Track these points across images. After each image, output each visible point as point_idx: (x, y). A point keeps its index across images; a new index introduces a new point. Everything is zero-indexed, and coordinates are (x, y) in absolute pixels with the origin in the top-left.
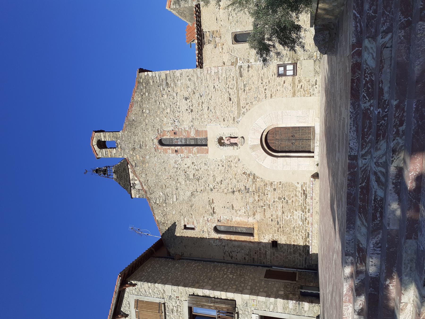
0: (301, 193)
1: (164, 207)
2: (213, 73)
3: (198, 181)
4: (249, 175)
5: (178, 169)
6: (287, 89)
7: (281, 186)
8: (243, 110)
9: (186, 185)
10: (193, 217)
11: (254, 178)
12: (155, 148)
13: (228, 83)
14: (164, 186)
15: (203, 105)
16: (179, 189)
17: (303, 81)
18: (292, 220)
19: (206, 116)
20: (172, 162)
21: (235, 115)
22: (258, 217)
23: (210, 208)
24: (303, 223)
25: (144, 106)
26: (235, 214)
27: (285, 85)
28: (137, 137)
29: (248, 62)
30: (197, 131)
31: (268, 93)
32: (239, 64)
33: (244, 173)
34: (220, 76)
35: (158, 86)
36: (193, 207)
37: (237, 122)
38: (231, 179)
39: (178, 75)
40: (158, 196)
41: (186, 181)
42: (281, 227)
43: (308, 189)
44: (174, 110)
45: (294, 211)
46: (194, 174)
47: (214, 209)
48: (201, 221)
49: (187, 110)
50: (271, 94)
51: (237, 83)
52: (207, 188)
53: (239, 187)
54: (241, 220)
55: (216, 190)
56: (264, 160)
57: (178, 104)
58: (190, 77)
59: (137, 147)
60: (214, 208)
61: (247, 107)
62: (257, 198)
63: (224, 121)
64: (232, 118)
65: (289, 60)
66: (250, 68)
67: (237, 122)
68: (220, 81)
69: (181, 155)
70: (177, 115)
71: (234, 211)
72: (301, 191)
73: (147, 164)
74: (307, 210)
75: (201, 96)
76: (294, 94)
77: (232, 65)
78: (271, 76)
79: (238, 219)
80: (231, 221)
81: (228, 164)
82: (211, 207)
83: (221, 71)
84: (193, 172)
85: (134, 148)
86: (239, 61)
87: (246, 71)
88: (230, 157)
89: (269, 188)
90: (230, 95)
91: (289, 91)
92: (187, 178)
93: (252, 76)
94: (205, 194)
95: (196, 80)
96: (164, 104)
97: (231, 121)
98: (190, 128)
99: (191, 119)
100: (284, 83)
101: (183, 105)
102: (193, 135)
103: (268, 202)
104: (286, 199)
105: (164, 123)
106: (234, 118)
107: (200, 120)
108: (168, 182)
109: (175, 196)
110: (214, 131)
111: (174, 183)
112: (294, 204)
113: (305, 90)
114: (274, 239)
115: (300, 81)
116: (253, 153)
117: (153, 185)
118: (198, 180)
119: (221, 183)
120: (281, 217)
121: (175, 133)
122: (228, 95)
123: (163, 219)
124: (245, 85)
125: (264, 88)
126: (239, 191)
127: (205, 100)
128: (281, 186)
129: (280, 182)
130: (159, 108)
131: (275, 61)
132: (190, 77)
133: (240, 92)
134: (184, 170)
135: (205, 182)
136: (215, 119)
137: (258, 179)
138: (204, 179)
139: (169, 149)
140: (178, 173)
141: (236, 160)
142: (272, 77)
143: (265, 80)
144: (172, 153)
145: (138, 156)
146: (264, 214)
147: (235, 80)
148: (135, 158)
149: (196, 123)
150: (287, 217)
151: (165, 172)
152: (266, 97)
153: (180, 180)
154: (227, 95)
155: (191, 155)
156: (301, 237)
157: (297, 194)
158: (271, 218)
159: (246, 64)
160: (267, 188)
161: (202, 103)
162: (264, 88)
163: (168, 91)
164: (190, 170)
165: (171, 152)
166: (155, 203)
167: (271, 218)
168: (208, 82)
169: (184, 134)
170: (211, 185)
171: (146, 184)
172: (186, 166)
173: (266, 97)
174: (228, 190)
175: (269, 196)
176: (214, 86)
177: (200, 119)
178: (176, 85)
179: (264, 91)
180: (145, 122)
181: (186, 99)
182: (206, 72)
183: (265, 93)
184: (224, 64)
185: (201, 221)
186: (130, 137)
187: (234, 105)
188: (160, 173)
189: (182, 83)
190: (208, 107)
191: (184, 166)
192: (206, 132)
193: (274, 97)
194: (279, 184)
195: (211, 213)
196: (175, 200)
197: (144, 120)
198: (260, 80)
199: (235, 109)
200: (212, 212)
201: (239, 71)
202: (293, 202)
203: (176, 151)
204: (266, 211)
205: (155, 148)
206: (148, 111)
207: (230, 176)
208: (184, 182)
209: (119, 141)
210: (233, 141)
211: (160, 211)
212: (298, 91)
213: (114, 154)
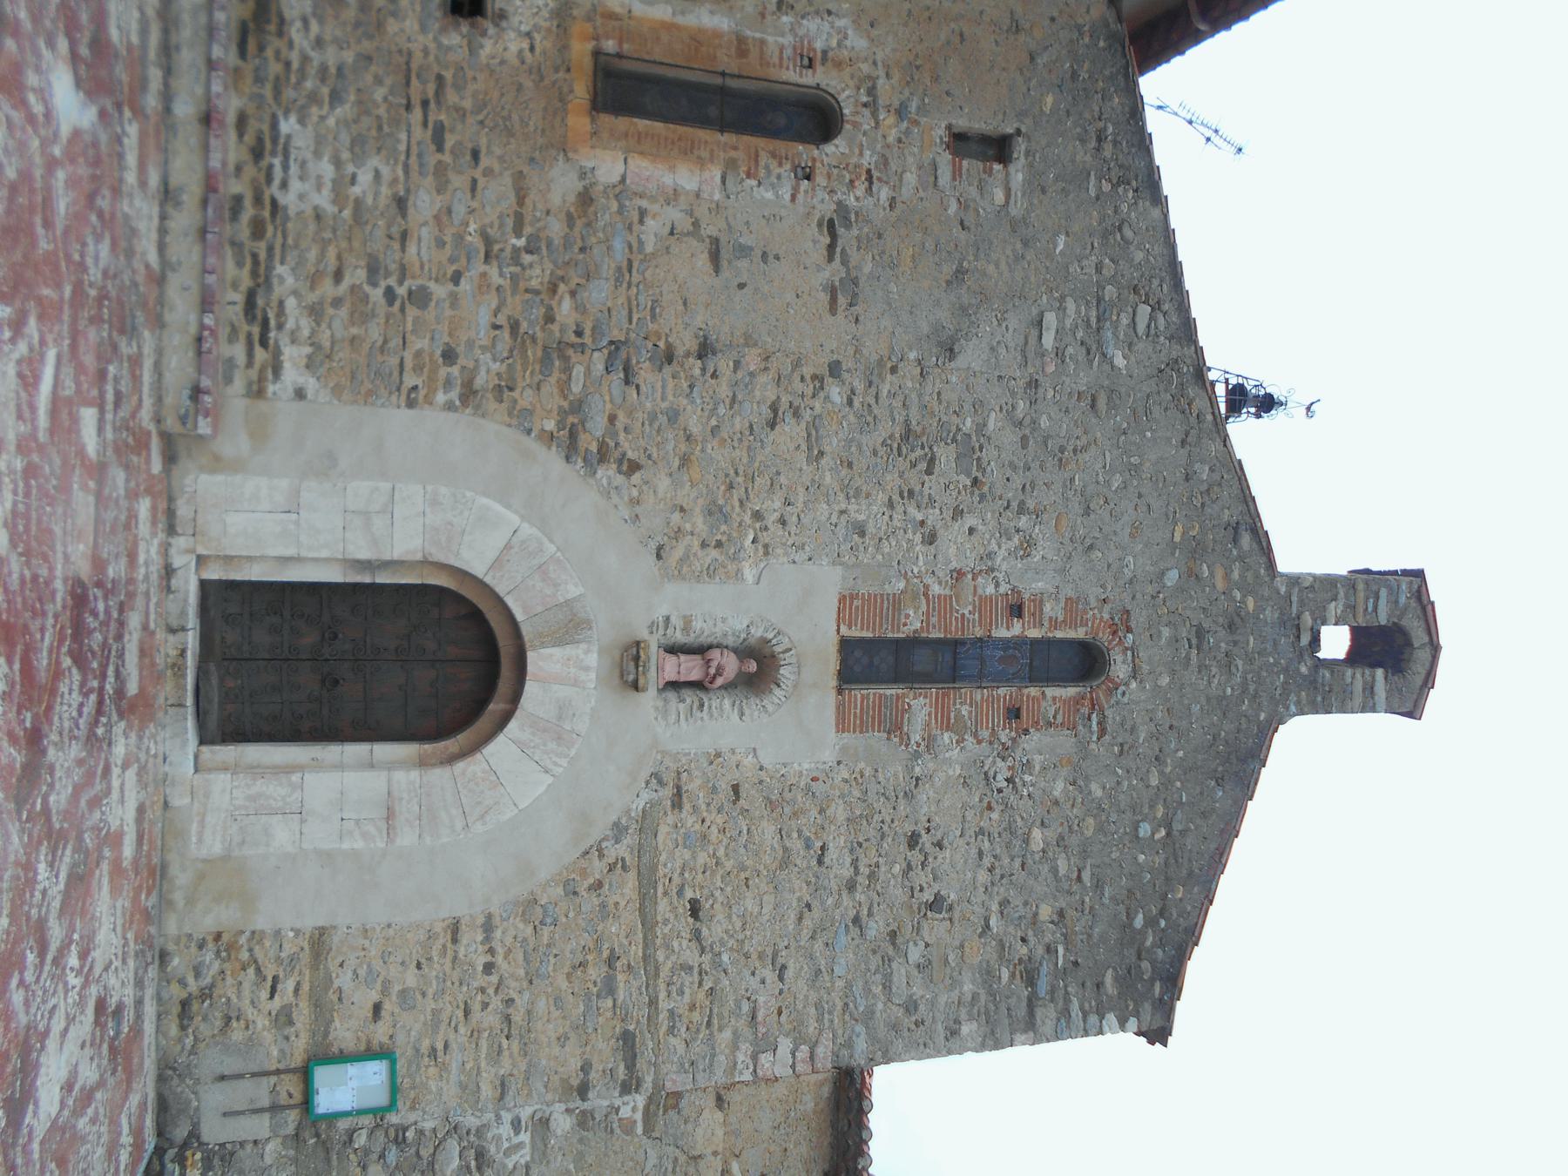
0: (280, 327)
1: (1113, 280)
2: (785, 1045)
3: (907, 422)
4: (603, 455)
5: (1014, 504)
6: (362, 972)
7: (410, 380)
8: (621, 850)
9: (978, 406)
10: (953, 207)
11: (573, 435)
12: (1129, 630)
13: (701, 995)
14: (1102, 403)
15: (847, 872)
16: (1021, 383)
17: (262, 1022)
18: (346, 155)
19: (839, 811)
20: (1045, 549)
21: (670, 819)
22: (561, 184)
23: (854, 256)
24: (274, 126)
25: (1158, 861)
26: (701, 211)
27: (374, 996)
28: (1214, 689)
29: (583, 1112)
30: (895, 728)
31: (471, 947)
32: (640, 1100)
33: (634, 467)
34: (747, 1032)
35: (1076, 964)
36: (948, 269)
37: (661, 782)
38: (715, 431)
39: (974, 1025)
40: (1140, 346)
41: (981, 427)
42: (417, 114)
43: (238, 352)
44: (1008, 846)
45: (330, 209)
46: (929, 472)
47: (831, 248)
48: (911, 178)
49: (939, 845)
50: (455, 941)
51: (653, 1002)
52: (859, 386)
53: (671, 383)
54: (672, 169)
55: (807, 371)
56: (508, 546)
57: (983, 876)
58: (908, 1022)
59: (1218, 640)
60: (830, 259)
61: (598, 867)
62: (565, 309)
63: (736, 789)
64: (687, 807)
65: (351, 1134)
66: (575, 1082)
67: (661, 782)
68: (746, 1007)
69: (990, 590)
70: (995, 816)
71: (711, 231)
72: (284, 341)
73: (1177, 538)
74: (248, 212)
75: (856, 920)
76: (319, 941)
77: (678, 1095)
78: (454, 1046)
79: (686, 178)
80: (731, 165)
81: (720, 533)
82: (844, 262)
83: (741, 1057)
84: (933, 485)
85: (1231, 627)
86: (639, 1116)
87: (597, 1067)
88: (711, 572)
89: (488, 371)
90: (697, 936)
91: (352, 962)
92: (969, 451)
93: (562, 1040)
94: (873, 349)
95: (880, 1006)
96: (1054, 871)
97: (693, 785)
98: (930, 742)
99: (925, 794)
100: (377, 1009)
101: (956, 870)
102: (920, 706)
103: (496, 279)
104: (377, 294)
105: (1064, 772)
106: (677, 803)
107: (873, 788)
108: (1079, 432)
109: (1049, 340)
110: (797, 732)
111: (1044, 422)
112: (332, 253)
113: (251, 971)
114: (465, 28)
115: (284, 1018)
116: (573, 590)
117: (1157, 412)
118: (908, 434)
119: (774, 408)
120: (414, 175)
121: (1014, 713)
122: (705, 932)
123: (1124, 208)
124: (609, 988)
125: (494, 979)
126: (669, 357)
127: (837, 905)
128: (410, 380)
129: (411, 404)
130: (1084, 854)
131: (428, 1125)
132: (908, 1022)
133: (636, 951)
134: (982, 497)
135: (867, 421)
136: (787, 796)
137: (550, 425)
138: (882, 432)
139: (1054, 624)
140: (1017, 481)
141: (679, 552)
142: (452, 1036)
143: (491, 1019)
144: (1039, 601)
145: (1220, 585)
146: (521, 201)
147: (663, 1016)
148: (1236, 575)
149: (894, 772)
150: (377, 175)
151: (1091, 488)
152: (488, 927)
153: (1010, 437)
154: (714, 931)
155: (936, 589)
156: (295, 32)
157: (306, 326)
158: (478, 174)
159: (598, 1101)
160: (496, 366)
161: (851, 886)
162: (494, 979)
163: (1032, 939)
164: (950, 500)
165: (1047, 608)
166: (1156, 308)
167: (478, 174)
168: (813, 996)
169: (965, 711)
170: (837, 399)
171: (1193, 420)
172: (970, 521)
173: (488, 927)
174: (737, 364)
175: (484, 317)
176: (781, 978)
177: (872, 796)
178: (988, 975)
179: (499, 959)
180: (1161, 773)
181: (936, 904)
182: (820, 1050)
183: (491, 951)
184: (719, 1099)
185: (911, 178)
186: (1245, 691)
187: (677, 880)
188: (1117, 482)
189: (955, 983)
190: (820, 862)
191: (982, 519)
192: (842, 725)
193: (438, 928)
194: (422, 393)
195: (848, 226)
196: (1050, 319)
197: (1166, 782)
198: (518, 1018)
199: (671, 860)
200: (841, 231)
201: (641, 1064)
202: (338, 276)
203: (1016, 610)
204: (510, 222)
205: (1129, 630)
206: (1145, 830)
207: (720, 455)
208: (991, 425)
209: (1304, 669)
210: (690, 668)
211: (1139, 256)
212: (293, 959)
213: (1335, 599)
